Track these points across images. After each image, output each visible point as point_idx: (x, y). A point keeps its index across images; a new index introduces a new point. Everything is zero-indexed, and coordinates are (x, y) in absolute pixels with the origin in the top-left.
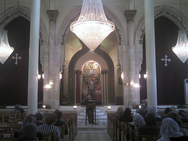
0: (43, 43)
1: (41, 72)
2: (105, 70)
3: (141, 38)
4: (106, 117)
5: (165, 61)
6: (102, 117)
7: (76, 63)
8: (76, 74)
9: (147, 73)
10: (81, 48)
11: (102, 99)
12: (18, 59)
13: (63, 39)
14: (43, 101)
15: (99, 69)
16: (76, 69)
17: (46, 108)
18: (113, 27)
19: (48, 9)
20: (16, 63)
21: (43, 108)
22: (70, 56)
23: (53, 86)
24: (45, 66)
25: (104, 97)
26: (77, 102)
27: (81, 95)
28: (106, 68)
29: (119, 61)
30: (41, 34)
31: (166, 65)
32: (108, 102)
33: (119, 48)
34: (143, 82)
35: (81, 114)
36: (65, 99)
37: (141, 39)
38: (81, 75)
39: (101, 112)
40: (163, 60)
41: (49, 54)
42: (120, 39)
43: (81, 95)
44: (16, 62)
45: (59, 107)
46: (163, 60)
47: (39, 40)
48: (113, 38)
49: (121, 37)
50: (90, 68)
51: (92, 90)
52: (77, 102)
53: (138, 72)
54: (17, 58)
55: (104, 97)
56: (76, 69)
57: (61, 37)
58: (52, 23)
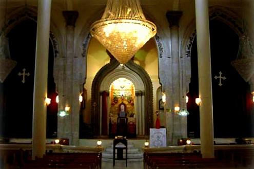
0: (58, 55)
1: (52, 95)
2: (141, 91)
3: (189, 49)
4: (141, 155)
5: (218, 79)
6: (136, 155)
7: (102, 81)
8: (101, 97)
9: (200, 96)
10: (108, 62)
11: (137, 129)
12: (26, 76)
13: (83, 49)
14: (57, 131)
15: (133, 90)
16: (102, 89)
17: (60, 143)
18: (153, 30)
19: (65, 10)
20: (23, 81)
21: (55, 143)
22: (93, 72)
23: (70, 112)
24: (59, 85)
25: (138, 128)
26: (103, 134)
27: (108, 123)
28: (142, 88)
29: (159, 78)
30: (52, 36)
31: (220, 84)
32: (145, 134)
33: (160, 61)
34: (193, 109)
35: (108, 150)
36: (88, 131)
37: (188, 50)
38: (108, 98)
39: (134, 147)
40: (20, 74)
41: (65, 70)
42: (161, 49)
43: (108, 123)
44: (22, 80)
45: (78, 141)
46: (20, 74)
47: (48, 41)
48: (150, 46)
49: (163, 46)
50: (121, 89)
51: (123, 118)
52: (103, 134)
53: (185, 94)
54: (24, 74)
55: (138, 128)
56: (102, 89)
57: (82, 47)
58: (70, 27)
